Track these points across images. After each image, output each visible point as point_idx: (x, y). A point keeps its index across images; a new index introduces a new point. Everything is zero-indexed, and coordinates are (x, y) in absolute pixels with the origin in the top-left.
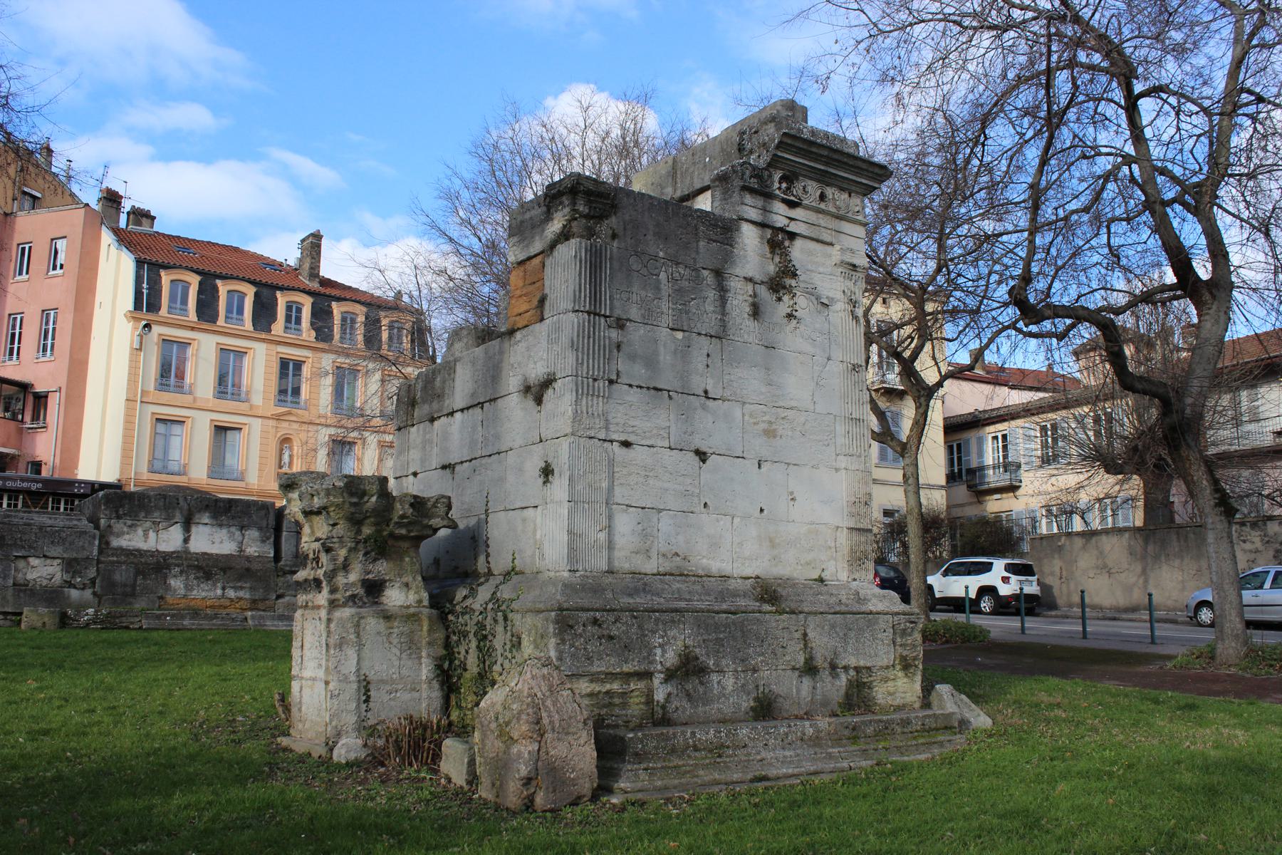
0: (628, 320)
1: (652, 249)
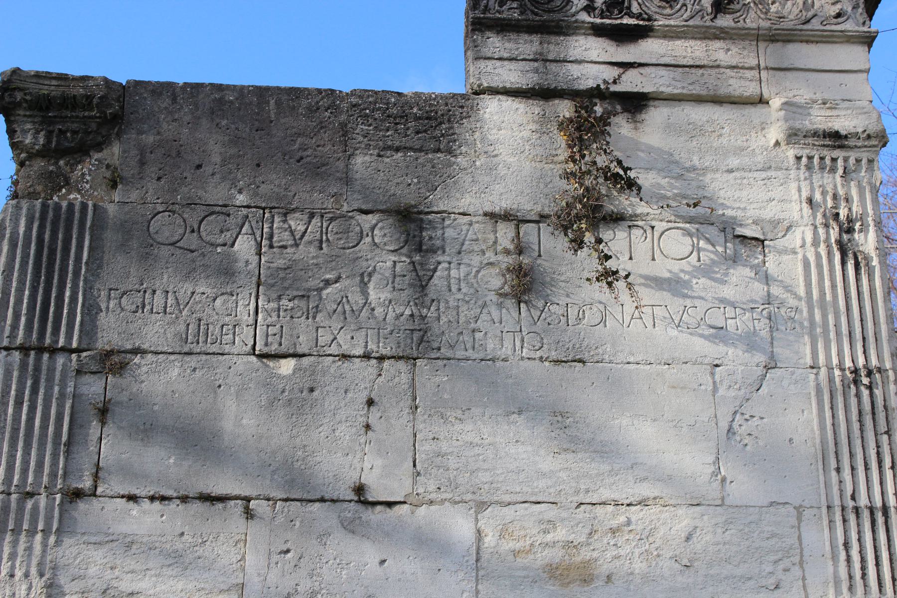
0: (136, 351)
1: (215, 192)
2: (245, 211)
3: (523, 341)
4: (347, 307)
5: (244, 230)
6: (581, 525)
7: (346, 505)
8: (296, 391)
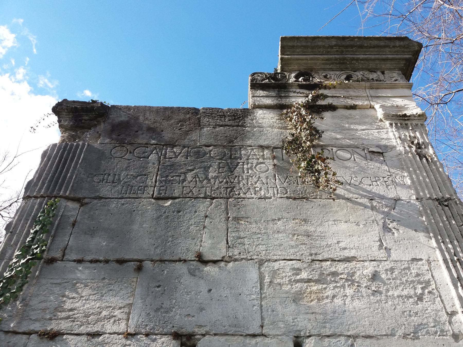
2: (154, 146)
3: (278, 190)
4: (197, 179)
5: (154, 152)
6: (315, 271)
7: (192, 262)
8: (171, 212)
